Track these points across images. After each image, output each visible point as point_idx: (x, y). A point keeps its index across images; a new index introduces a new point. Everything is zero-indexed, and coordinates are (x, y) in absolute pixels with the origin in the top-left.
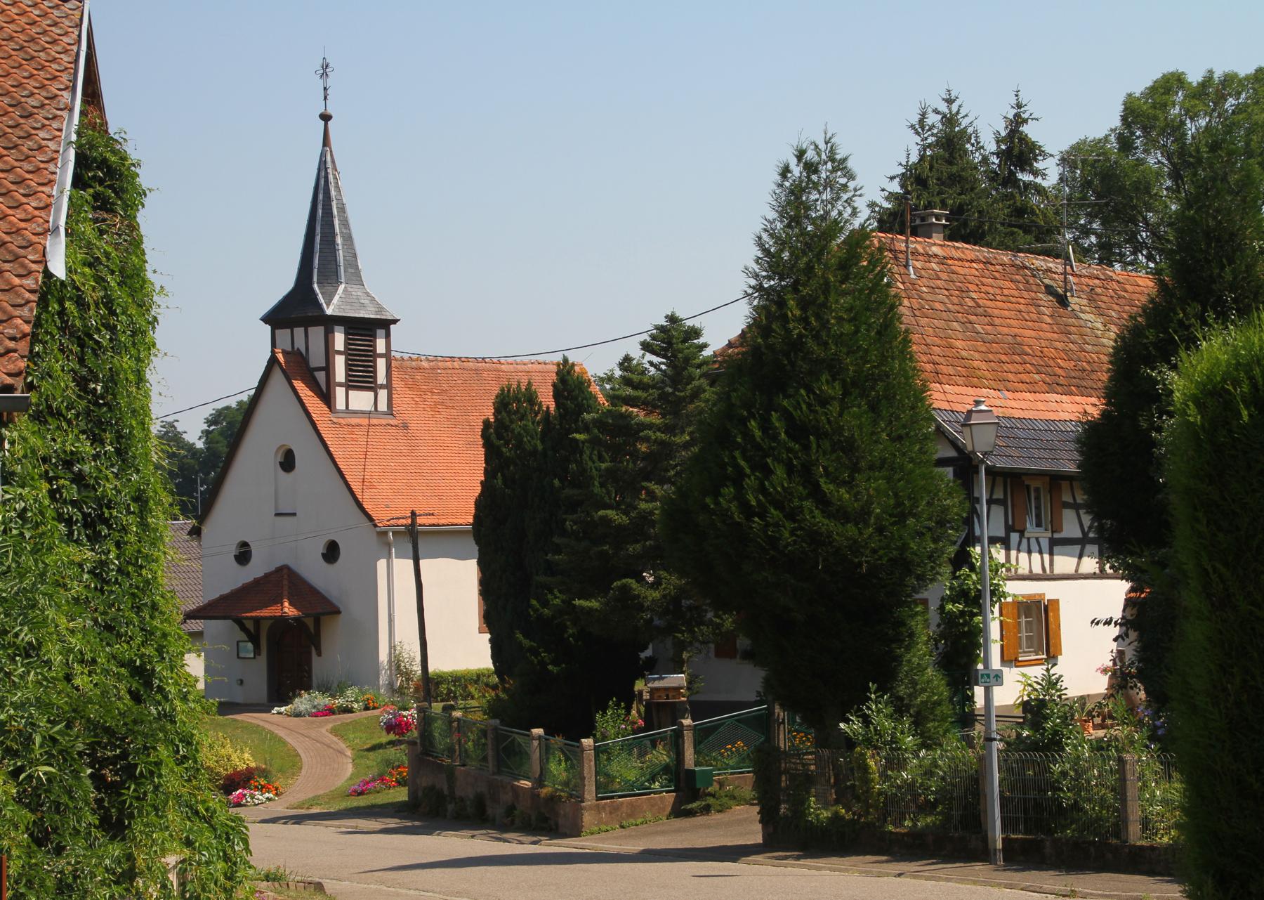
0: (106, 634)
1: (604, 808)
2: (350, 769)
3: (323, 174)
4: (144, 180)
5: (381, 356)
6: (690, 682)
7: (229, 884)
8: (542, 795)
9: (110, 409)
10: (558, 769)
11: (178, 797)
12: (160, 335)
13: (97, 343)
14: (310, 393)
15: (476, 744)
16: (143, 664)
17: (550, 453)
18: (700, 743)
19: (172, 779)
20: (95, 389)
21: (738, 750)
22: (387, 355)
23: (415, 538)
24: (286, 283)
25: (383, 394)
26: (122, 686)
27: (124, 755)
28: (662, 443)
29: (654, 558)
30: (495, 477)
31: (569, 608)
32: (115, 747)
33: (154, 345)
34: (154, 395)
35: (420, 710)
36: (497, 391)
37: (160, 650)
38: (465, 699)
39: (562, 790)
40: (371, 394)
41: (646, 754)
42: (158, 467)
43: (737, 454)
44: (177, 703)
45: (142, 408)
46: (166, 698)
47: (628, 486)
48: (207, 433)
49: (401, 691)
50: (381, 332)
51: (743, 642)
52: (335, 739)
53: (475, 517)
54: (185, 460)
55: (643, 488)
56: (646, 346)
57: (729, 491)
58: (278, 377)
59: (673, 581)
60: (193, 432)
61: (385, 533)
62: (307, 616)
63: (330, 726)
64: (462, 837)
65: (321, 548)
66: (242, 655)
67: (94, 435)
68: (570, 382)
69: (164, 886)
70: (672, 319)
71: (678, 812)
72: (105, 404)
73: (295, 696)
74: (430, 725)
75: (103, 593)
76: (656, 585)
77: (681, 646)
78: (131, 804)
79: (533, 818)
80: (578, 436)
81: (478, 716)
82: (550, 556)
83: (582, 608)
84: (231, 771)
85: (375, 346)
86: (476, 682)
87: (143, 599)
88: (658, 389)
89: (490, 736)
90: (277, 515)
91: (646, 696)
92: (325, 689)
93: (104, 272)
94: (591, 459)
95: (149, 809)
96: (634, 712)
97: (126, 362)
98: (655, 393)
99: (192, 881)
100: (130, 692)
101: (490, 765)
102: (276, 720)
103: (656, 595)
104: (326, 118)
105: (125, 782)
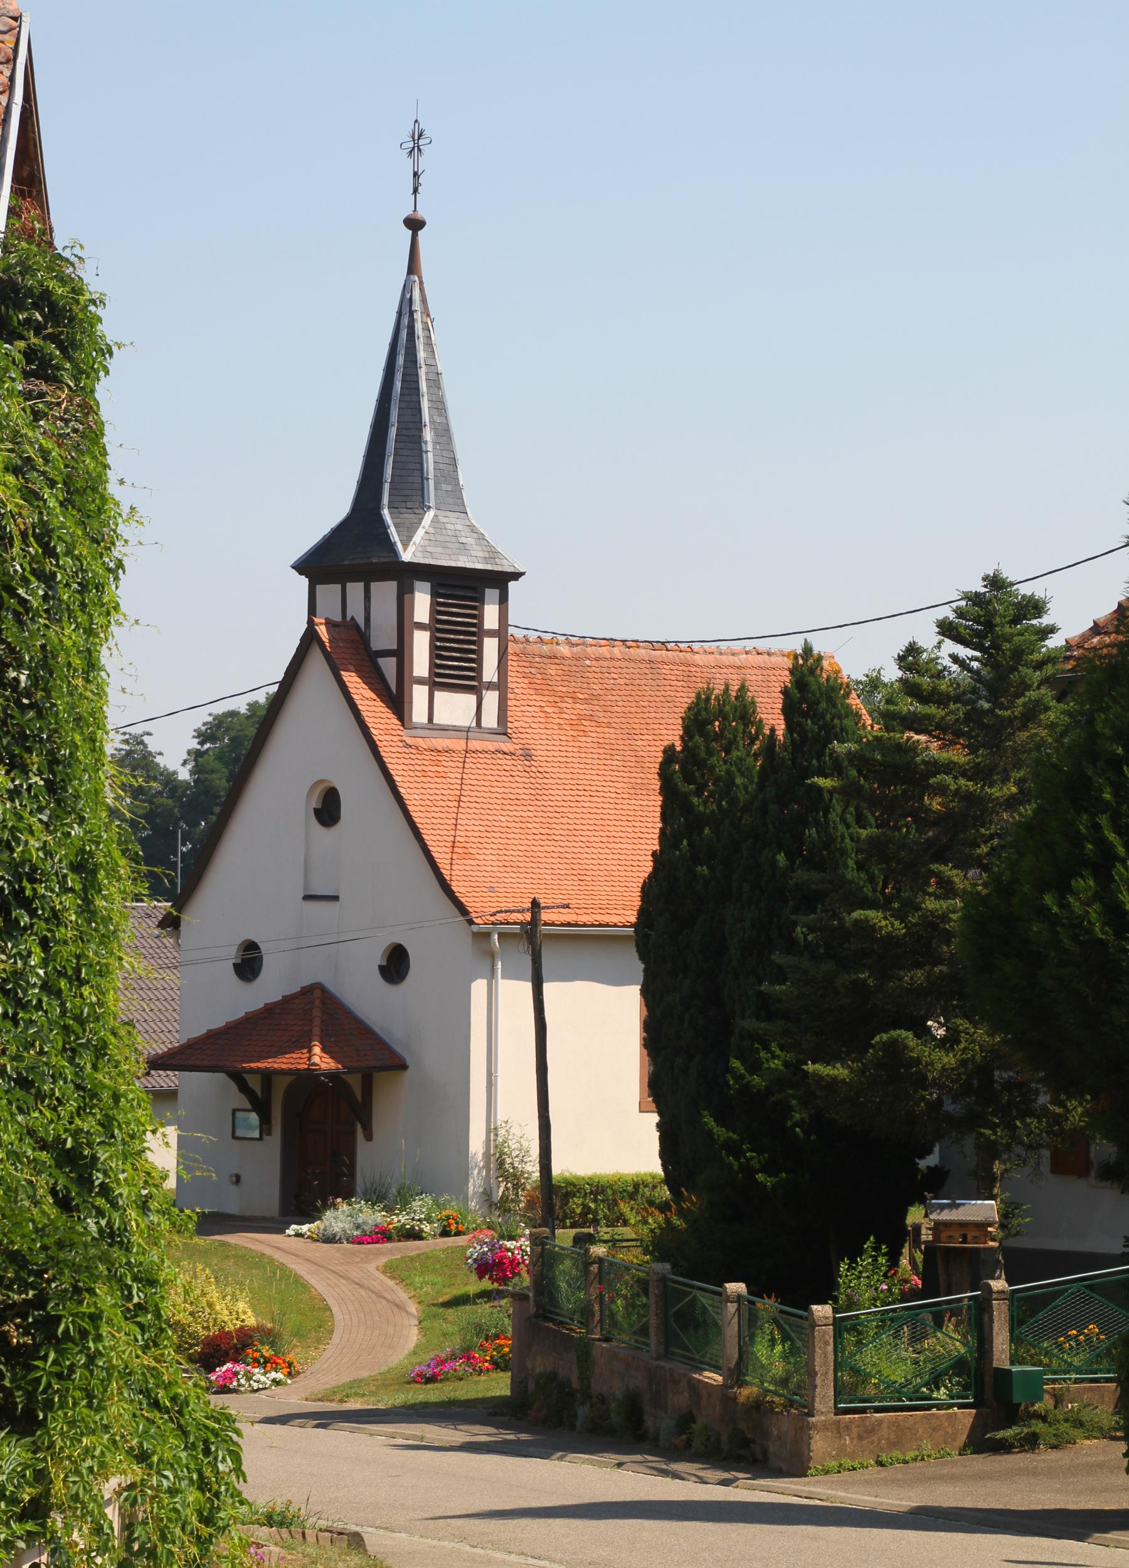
0: (19, 1093)
1: (848, 1428)
2: (413, 1336)
3: (405, 321)
4: (111, 326)
5: (491, 633)
6: (1005, 1215)
7: (205, 1531)
8: (741, 1400)
9: (40, 715)
10: (770, 1356)
11: (127, 1374)
12: (127, 592)
13: (23, 602)
14: (370, 694)
15: (630, 1305)
16: (77, 1146)
17: (773, 808)
18: (1021, 1323)
19: (119, 1343)
20: (16, 680)
21: (1088, 1339)
22: (501, 634)
23: (537, 945)
24: (335, 506)
25: (491, 699)
26: (43, 1182)
27: (40, 1301)
28: (968, 798)
29: (947, 995)
30: (676, 846)
31: (795, 1074)
32: (25, 1287)
33: (116, 608)
34: (112, 692)
35: (535, 1240)
36: (686, 699)
37: (107, 1124)
38: (611, 1224)
39: (775, 1393)
40: (472, 699)
41: (925, 1336)
42: (113, 813)
43: (1103, 820)
44: (132, 1213)
45: (92, 714)
46: (114, 1205)
47: (904, 869)
48: (196, 755)
49: (504, 1206)
50: (491, 594)
51: (1103, 1149)
52: (391, 1283)
53: (642, 913)
54: (159, 800)
55: (933, 873)
56: (946, 629)
57: (1085, 884)
58: (317, 664)
59: (979, 1037)
60: (174, 751)
61: (487, 935)
62: (351, 1071)
63: (383, 1260)
64: (601, 1465)
65: (377, 956)
66: (240, 1133)
67: (12, 757)
68: (814, 687)
69: (98, 1530)
70: (996, 582)
71: (980, 1443)
72: (31, 706)
73: (326, 1206)
74: (551, 1267)
75: (16, 1023)
76: (950, 1042)
77: (991, 1151)
78: (49, 1385)
79: (724, 1438)
80: (822, 782)
81: (633, 1256)
82: (765, 987)
83: (818, 1078)
84: (214, 1331)
85: (480, 617)
86: (632, 1196)
87: (82, 1038)
88: (965, 703)
89: (654, 1290)
90: (308, 898)
91: (926, 1236)
92: (377, 1197)
93: (37, 483)
94: (844, 820)
95: (78, 1394)
96: (904, 1261)
97: (70, 635)
98: (959, 710)
99: (145, 1523)
100: (53, 1192)
101: (653, 1340)
102: (290, 1247)
103: (949, 1060)
104: (414, 224)
105: (40, 1345)
